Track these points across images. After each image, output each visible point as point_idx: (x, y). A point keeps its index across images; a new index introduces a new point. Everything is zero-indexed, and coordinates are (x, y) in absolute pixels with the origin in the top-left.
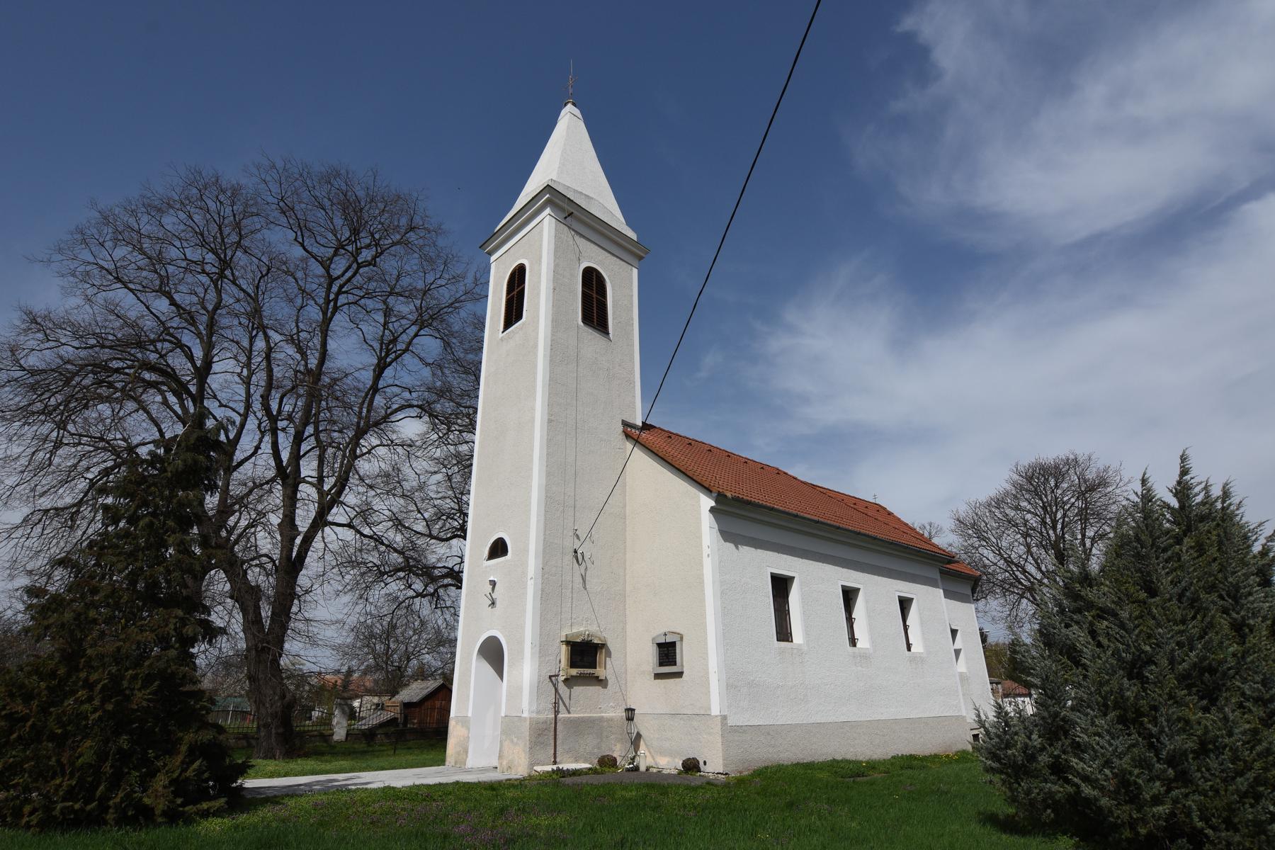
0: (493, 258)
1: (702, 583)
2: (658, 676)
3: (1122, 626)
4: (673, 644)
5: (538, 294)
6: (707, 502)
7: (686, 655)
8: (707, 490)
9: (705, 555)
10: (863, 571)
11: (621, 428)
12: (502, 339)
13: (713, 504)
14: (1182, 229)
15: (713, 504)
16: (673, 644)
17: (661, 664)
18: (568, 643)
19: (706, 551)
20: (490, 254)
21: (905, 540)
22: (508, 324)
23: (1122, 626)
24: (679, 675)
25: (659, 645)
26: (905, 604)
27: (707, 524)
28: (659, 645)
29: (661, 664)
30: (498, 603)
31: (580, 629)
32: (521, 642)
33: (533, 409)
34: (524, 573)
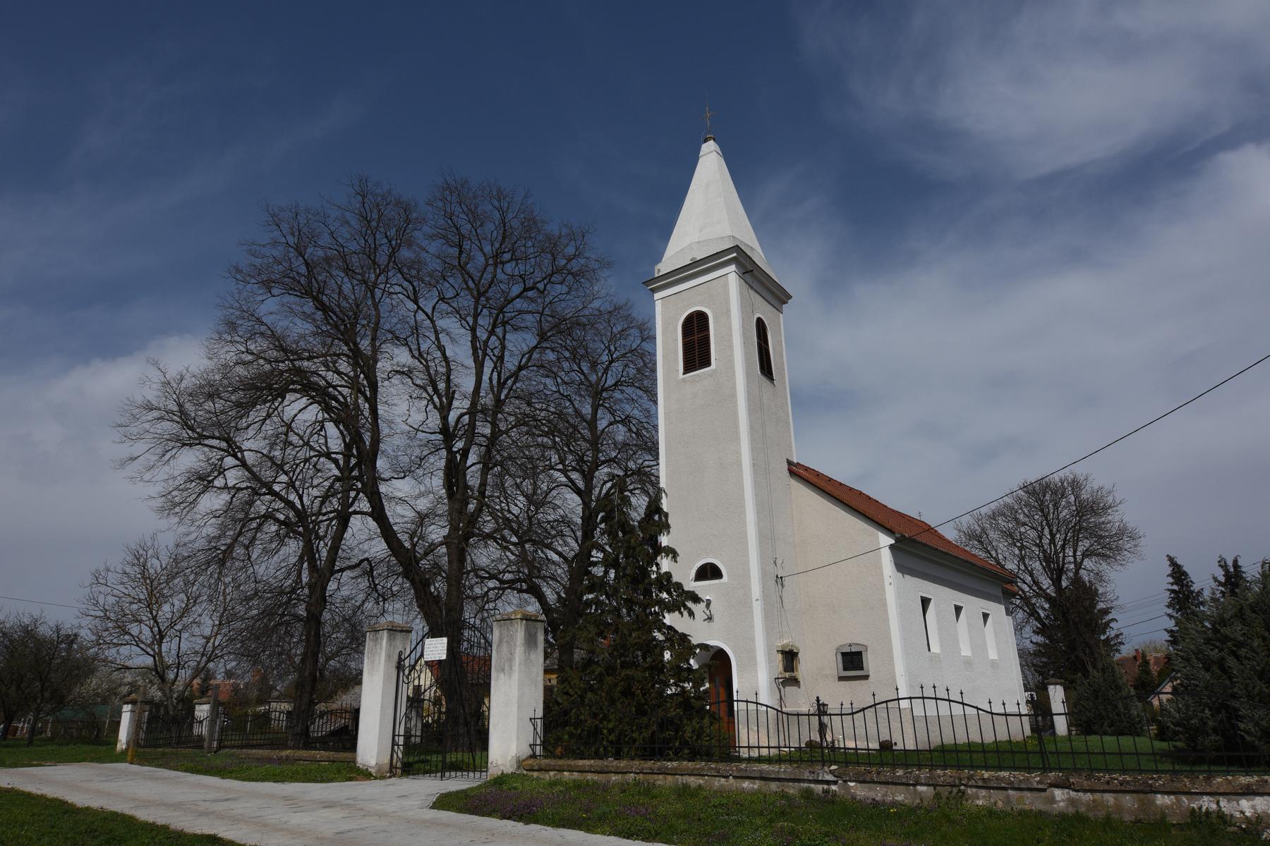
0: (657, 296)
1: (885, 605)
2: (841, 679)
3: (1254, 651)
4: (860, 653)
5: (731, 347)
6: (886, 540)
7: (870, 662)
8: (889, 531)
9: (887, 584)
10: (934, 582)
11: (786, 466)
12: (683, 380)
13: (893, 542)
14: (1157, 171)
15: (893, 542)
16: (860, 653)
17: (845, 669)
18: (782, 652)
19: (887, 580)
20: (653, 291)
21: (933, 543)
22: (690, 366)
23: (1254, 651)
24: (866, 677)
25: (843, 654)
26: (925, 602)
27: (886, 557)
28: (843, 654)
29: (845, 669)
30: (715, 618)
31: (784, 642)
32: (751, 652)
33: (738, 453)
34: (748, 594)
